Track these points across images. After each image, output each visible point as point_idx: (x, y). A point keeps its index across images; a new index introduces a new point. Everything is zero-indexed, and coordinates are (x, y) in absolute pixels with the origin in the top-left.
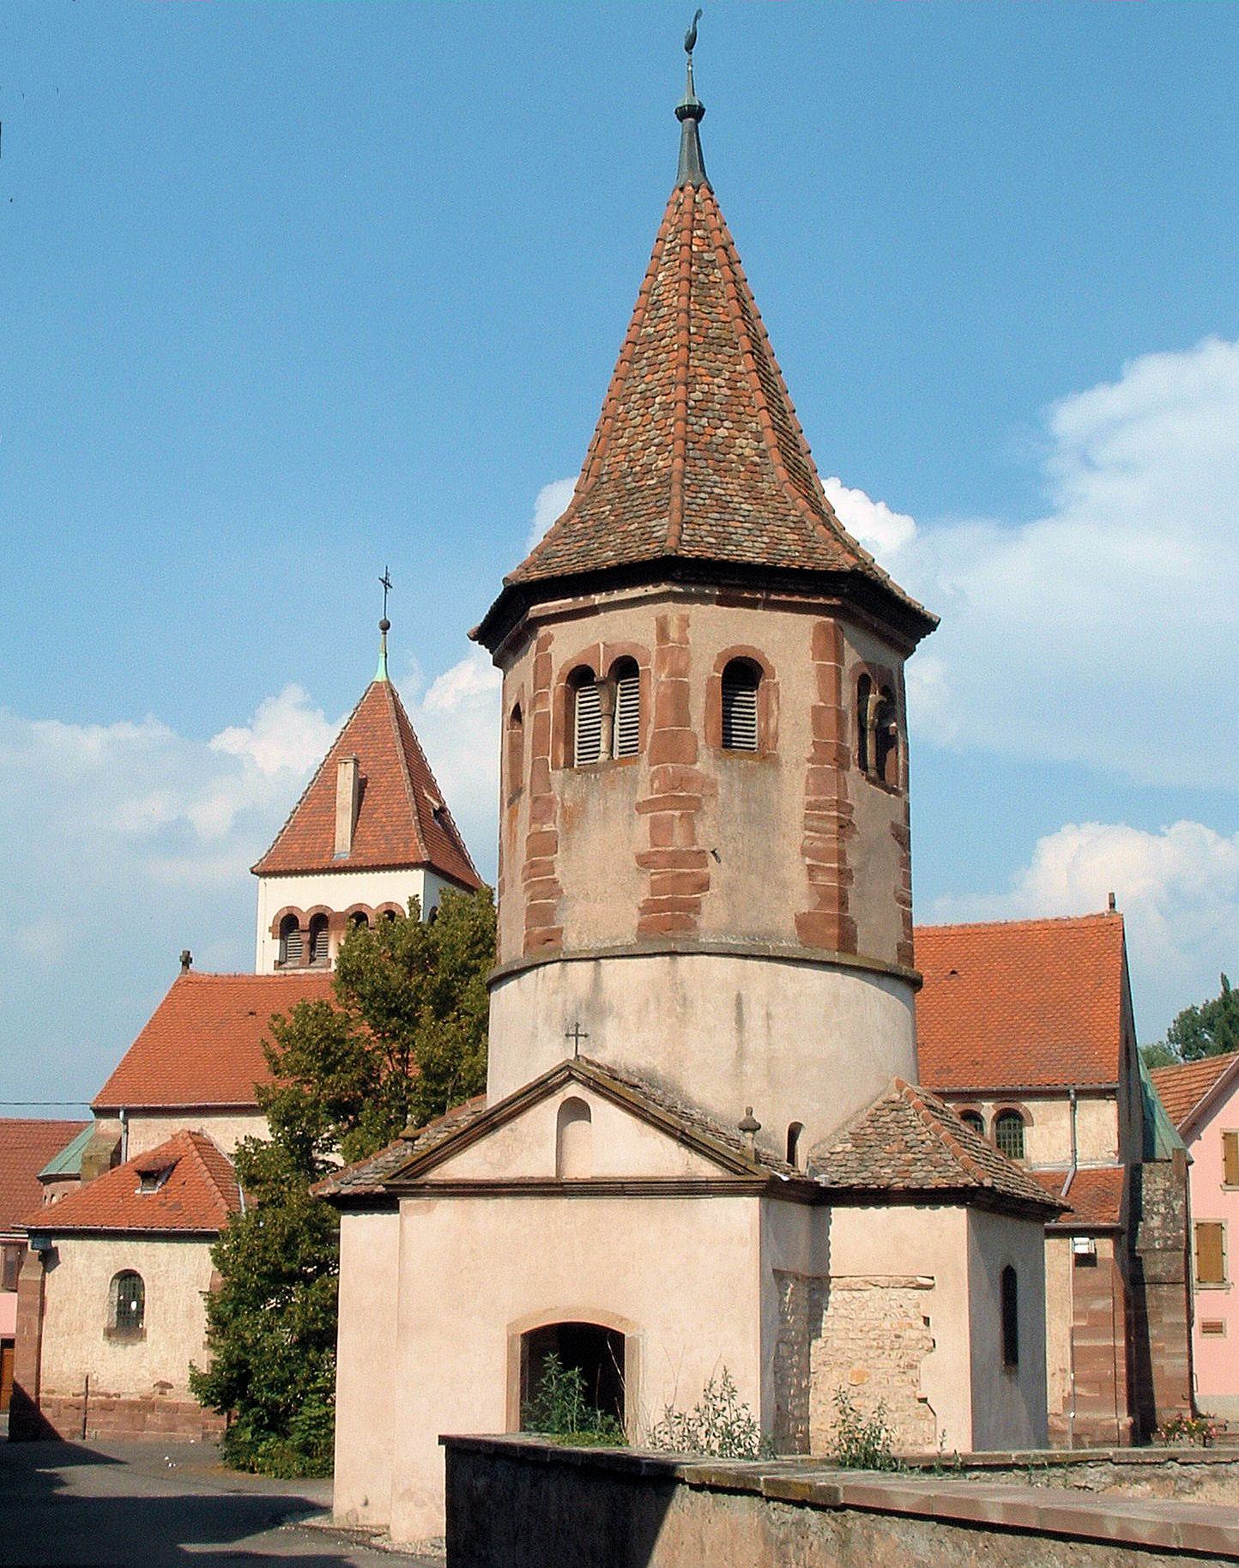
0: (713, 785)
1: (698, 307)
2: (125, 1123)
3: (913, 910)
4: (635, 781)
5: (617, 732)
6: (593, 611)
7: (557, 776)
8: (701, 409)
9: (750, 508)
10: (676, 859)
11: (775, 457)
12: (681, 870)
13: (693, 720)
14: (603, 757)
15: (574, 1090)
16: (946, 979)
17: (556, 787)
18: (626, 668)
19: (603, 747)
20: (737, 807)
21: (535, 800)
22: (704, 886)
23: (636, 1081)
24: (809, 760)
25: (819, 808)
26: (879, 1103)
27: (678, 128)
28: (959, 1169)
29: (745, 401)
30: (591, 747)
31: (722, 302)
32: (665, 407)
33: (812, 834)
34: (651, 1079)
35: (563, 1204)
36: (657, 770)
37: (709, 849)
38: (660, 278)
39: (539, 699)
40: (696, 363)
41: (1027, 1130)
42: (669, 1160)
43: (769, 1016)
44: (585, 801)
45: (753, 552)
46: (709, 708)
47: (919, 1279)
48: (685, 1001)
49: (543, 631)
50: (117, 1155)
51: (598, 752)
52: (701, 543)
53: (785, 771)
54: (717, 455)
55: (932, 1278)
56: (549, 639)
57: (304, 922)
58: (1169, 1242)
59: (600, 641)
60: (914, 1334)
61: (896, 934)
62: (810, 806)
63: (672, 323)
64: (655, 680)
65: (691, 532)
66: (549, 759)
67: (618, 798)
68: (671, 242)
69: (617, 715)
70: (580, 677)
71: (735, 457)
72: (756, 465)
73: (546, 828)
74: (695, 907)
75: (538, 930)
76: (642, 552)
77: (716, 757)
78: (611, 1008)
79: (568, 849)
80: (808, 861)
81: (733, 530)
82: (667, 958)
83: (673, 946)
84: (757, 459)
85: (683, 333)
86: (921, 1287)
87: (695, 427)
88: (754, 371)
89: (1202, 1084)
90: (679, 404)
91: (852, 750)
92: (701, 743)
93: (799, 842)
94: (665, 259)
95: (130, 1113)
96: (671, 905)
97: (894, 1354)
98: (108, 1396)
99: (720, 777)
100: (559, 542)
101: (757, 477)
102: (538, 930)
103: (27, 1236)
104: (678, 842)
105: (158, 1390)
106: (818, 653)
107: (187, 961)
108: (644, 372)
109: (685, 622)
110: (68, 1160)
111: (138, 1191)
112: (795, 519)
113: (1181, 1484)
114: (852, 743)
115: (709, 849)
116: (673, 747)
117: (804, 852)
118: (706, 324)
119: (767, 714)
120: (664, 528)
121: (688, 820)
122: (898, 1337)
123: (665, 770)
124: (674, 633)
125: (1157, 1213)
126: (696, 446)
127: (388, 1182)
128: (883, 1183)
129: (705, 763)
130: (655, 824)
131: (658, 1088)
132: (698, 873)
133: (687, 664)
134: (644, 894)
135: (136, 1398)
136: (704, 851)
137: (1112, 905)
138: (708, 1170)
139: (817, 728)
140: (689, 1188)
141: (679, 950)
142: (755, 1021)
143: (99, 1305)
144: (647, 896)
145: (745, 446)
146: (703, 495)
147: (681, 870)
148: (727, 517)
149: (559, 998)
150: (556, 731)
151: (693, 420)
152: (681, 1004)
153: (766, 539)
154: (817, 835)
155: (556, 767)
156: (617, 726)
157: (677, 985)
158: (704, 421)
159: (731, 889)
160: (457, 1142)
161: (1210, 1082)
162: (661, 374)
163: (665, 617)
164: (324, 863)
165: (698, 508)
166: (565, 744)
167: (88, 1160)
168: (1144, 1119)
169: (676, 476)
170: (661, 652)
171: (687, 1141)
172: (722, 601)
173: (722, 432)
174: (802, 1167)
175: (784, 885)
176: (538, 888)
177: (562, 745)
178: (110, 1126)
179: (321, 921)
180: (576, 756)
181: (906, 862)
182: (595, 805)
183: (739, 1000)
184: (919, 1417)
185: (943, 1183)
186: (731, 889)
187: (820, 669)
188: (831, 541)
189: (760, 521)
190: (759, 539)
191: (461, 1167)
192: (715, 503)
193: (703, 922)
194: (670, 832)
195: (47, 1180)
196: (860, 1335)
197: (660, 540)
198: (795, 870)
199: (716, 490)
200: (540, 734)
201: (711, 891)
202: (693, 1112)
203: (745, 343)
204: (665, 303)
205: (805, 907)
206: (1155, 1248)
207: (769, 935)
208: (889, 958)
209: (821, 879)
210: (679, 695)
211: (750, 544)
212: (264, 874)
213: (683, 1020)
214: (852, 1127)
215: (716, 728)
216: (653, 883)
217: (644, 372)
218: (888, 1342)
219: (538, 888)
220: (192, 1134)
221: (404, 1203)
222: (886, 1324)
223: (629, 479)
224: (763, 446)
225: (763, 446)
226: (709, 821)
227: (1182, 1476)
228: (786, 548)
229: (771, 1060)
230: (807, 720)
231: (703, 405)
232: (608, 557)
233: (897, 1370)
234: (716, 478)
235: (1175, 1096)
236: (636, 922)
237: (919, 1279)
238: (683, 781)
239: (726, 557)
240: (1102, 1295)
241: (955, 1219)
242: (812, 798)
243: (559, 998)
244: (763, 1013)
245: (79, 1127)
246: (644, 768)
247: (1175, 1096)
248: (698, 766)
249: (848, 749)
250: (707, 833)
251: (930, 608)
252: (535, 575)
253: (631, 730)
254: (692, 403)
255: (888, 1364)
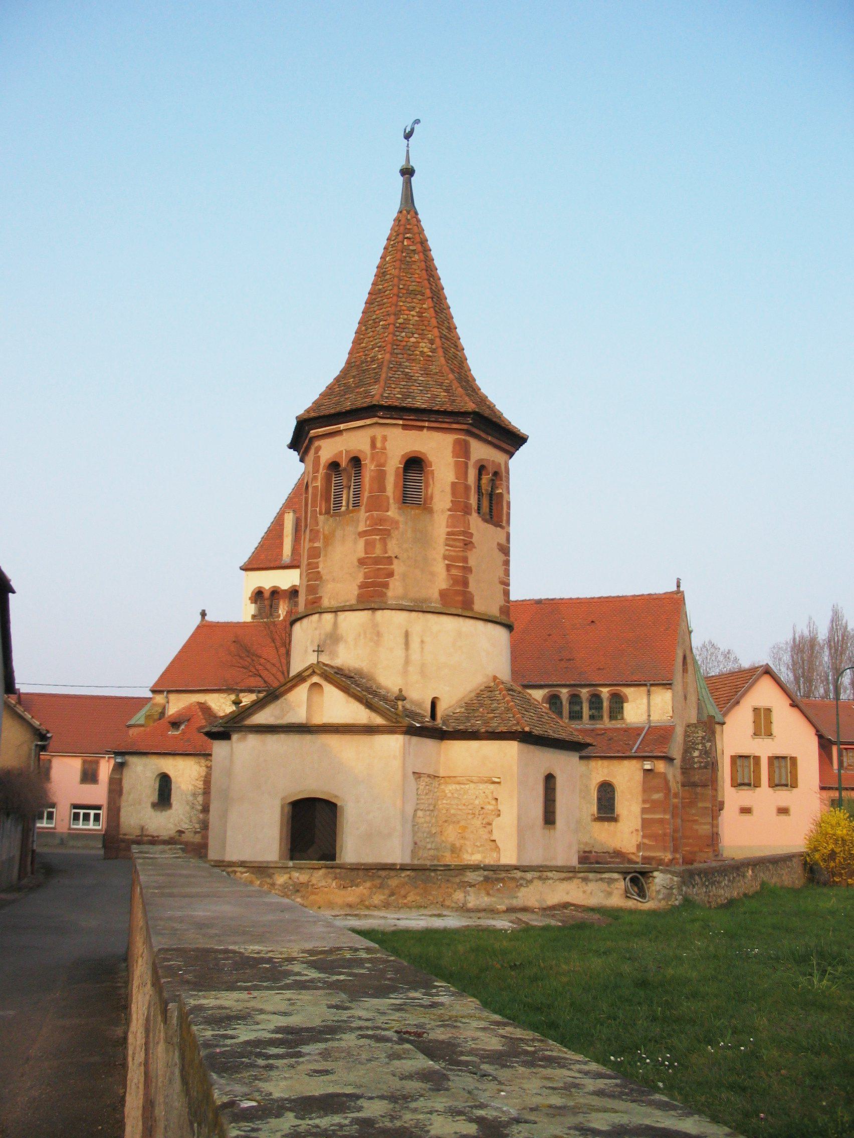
0: (397, 522)
1: (404, 274)
2: (167, 697)
3: (511, 588)
4: (358, 521)
5: (351, 496)
6: (340, 432)
7: (321, 518)
8: (402, 328)
9: (423, 379)
10: (377, 561)
11: (440, 352)
12: (378, 567)
13: (388, 490)
14: (343, 509)
15: (316, 679)
16: (588, 625)
17: (321, 524)
18: (356, 461)
19: (344, 503)
20: (409, 534)
21: (311, 530)
22: (391, 574)
23: (353, 675)
24: (449, 510)
25: (453, 535)
26: (483, 688)
27: (400, 179)
28: (515, 722)
29: (426, 323)
30: (338, 504)
31: (418, 271)
32: (385, 327)
33: (449, 548)
34: (360, 673)
35: (308, 738)
36: (369, 515)
37: (393, 556)
38: (387, 259)
39: (315, 478)
40: (401, 304)
41: (625, 705)
42: (357, 713)
43: (422, 642)
44: (334, 531)
45: (419, 404)
46: (396, 485)
47: (493, 779)
48: (378, 634)
49: (317, 444)
50: (163, 714)
51: (341, 506)
52: (395, 397)
53: (435, 515)
54: (409, 351)
55: (500, 778)
56: (318, 449)
57: (267, 595)
58: (702, 764)
59: (343, 448)
60: (491, 807)
61: (500, 601)
62: (448, 534)
63: (391, 283)
64: (369, 468)
65: (390, 392)
66: (318, 509)
67: (350, 529)
68: (393, 240)
69: (352, 487)
70: (334, 466)
71: (418, 353)
72: (430, 356)
73: (316, 545)
74: (386, 585)
75: (310, 597)
76: (362, 402)
77: (400, 509)
78: (342, 637)
79: (325, 556)
80: (447, 562)
81: (412, 391)
82: (370, 612)
83: (373, 606)
84: (430, 354)
85: (396, 288)
86: (494, 783)
87: (398, 337)
88: (432, 307)
89: (743, 682)
90: (391, 326)
91: (473, 506)
92: (391, 501)
93: (442, 552)
94: (391, 249)
95: (169, 692)
96: (373, 584)
97: (480, 817)
98: (153, 837)
99: (401, 519)
100: (327, 398)
101: (430, 363)
102: (310, 597)
103: (113, 756)
104: (378, 552)
105: (178, 834)
106: (455, 454)
107: (203, 614)
108: (375, 309)
109: (385, 439)
110: (139, 718)
111: (170, 733)
112: (447, 385)
113: (521, 882)
114: (473, 501)
115: (393, 556)
116: (378, 503)
117: (445, 558)
118: (408, 283)
119: (427, 486)
120: (376, 390)
121: (384, 541)
122: (482, 808)
123: (372, 515)
124: (379, 445)
125: (697, 749)
126: (398, 347)
127: (225, 725)
128: (475, 728)
129: (393, 512)
130: (367, 543)
131: (363, 678)
132: (387, 568)
133: (385, 461)
134: (360, 578)
135: (166, 838)
136: (391, 557)
137: (678, 586)
138: (379, 720)
139: (454, 493)
140: (369, 730)
141: (376, 608)
142: (415, 644)
143: (148, 790)
144: (361, 580)
145: (424, 347)
146: (399, 373)
147: (378, 567)
148: (410, 384)
149: (317, 632)
150: (321, 496)
151: (398, 333)
152: (377, 635)
153: (429, 396)
154: (452, 549)
155: (321, 514)
156: (351, 493)
157: (375, 625)
158: (403, 334)
159: (404, 576)
160: (257, 705)
161: (747, 681)
162: (383, 310)
163: (374, 436)
164: (277, 564)
165: (395, 379)
166: (326, 503)
167: (148, 717)
168: (699, 699)
169: (385, 363)
170: (372, 454)
171: (369, 706)
172: (405, 427)
173: (412, 340)
174: (439, 721)
175: (432, 574)
176: (311, 575)
177: (324, 503)
178: (160, 699)
179: (275, 593)
180: (332, 508)
181: (507, 563)
182: (339, 533)
183: (407, 635)
184: (491, 849)
185: (505, 729)
186: (404, 576)
187: (456, 463)
188: (464, 396)
189: (428, 386)
190: (426, 395)
191: (262, 717)
192: (404, 376)
193: (390, 593)
194: (374, 547)
195: (129, 726)
196: (464, 807)
197: (373, 396)
198: (440, 568)
199: (407, 370)
200: (315, 496)
201: (394, 577)
202: (381, 691)
203: (428, 293)
204: (389, 272)
205: (444, 586)
206: (694, 767)
207: (425, 600)
208: (495, 611)
209: (454, 572)
210: (381, 476)
211: (420, 398)
212: (243, 570)
213: (377, 643)
214: (466, 700)
215: (399, 494)
216: (365, 573)
217: (375, 309)
218: (477, 811)
219: (311, 575)
220: (199, 704)
221: (235, 737)
222: (477, 802)
223: (364, 365)
224: (434, 346)
225: (434, 346)
226: (394, 541)
227: (522, 878)
228: (439, 400)
229: (423, 665)
230: (448, 489)
231: (404, 326)
232: (348, 406)
233: (482, 825)
234: (407, 364)
235: (730, 688)
236: (356, 593)
237: (493, 779)
238: (381, 521)
239: (405, 405)
240: (658, 792)
241: (512, 748)
242: (449, 530)
243: (317, 632)
244: (419, 640)
245: (148, 700)
246: (363, 514)
247: (730, 688)
248: (389, 513)
249: (471, 504)
250: (393, 547)
251: (523, 430)
252: (313, 415)
253: (357, 495)
254: (398, 325)
255: (477, 822)
